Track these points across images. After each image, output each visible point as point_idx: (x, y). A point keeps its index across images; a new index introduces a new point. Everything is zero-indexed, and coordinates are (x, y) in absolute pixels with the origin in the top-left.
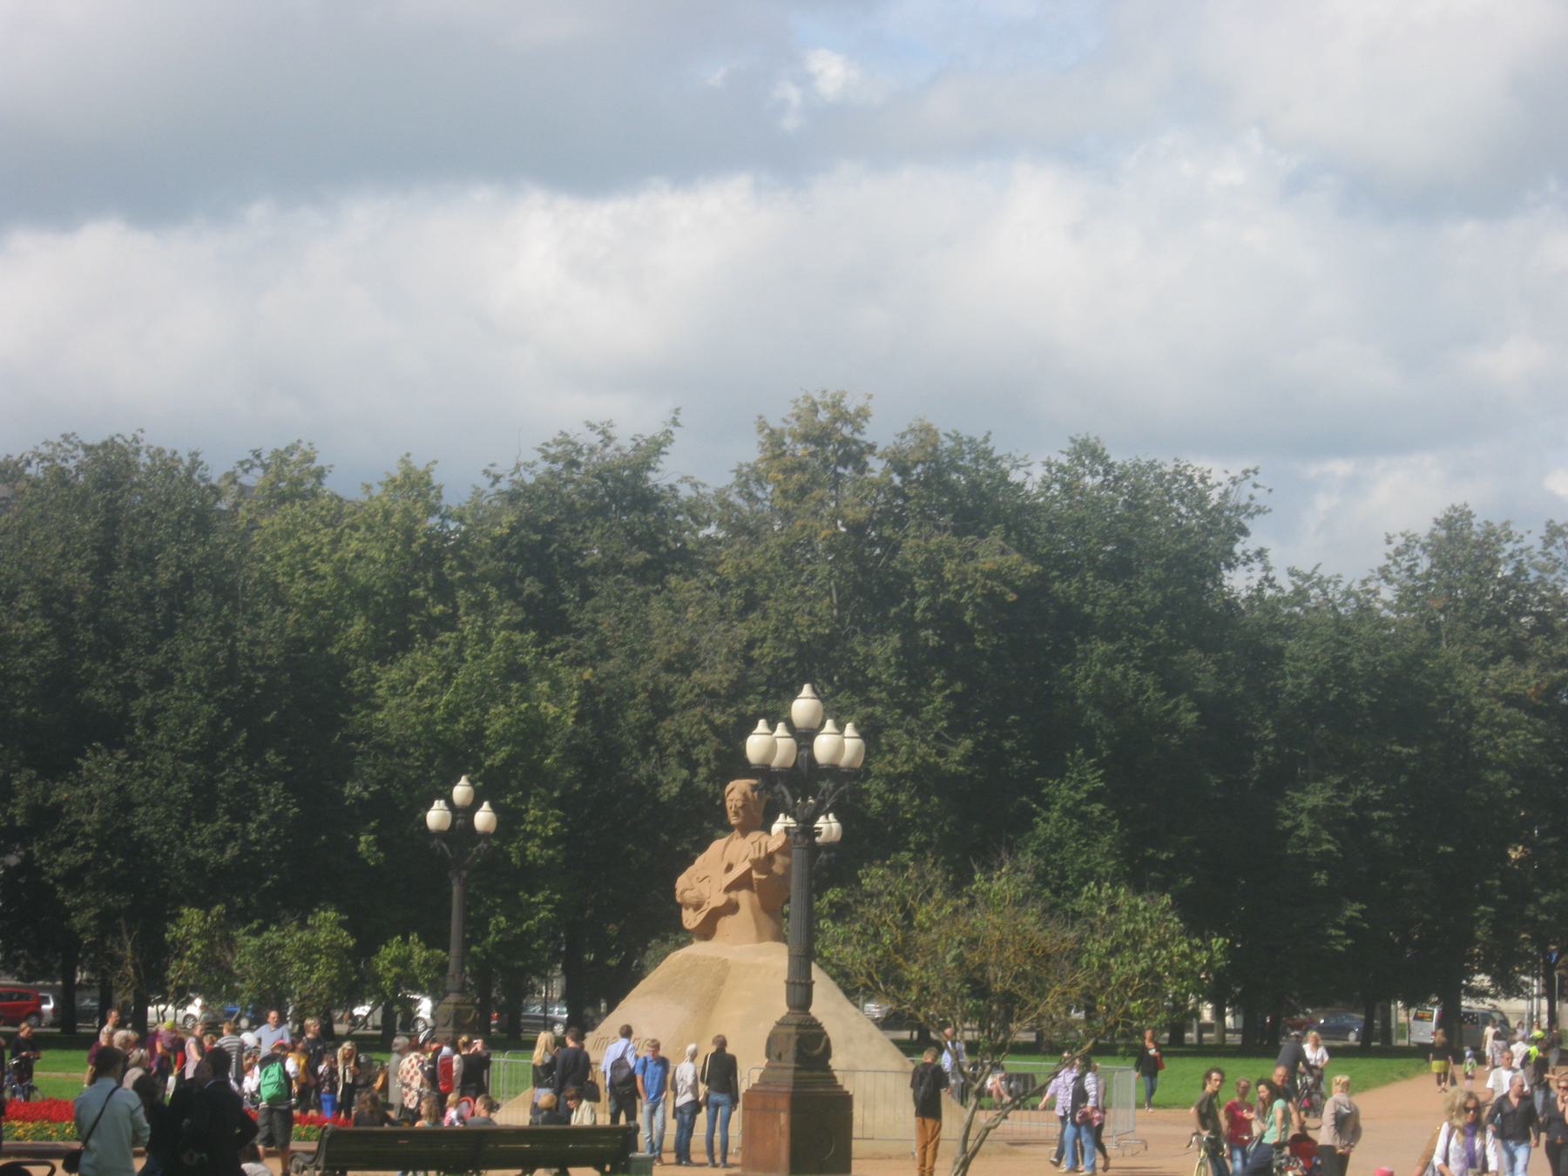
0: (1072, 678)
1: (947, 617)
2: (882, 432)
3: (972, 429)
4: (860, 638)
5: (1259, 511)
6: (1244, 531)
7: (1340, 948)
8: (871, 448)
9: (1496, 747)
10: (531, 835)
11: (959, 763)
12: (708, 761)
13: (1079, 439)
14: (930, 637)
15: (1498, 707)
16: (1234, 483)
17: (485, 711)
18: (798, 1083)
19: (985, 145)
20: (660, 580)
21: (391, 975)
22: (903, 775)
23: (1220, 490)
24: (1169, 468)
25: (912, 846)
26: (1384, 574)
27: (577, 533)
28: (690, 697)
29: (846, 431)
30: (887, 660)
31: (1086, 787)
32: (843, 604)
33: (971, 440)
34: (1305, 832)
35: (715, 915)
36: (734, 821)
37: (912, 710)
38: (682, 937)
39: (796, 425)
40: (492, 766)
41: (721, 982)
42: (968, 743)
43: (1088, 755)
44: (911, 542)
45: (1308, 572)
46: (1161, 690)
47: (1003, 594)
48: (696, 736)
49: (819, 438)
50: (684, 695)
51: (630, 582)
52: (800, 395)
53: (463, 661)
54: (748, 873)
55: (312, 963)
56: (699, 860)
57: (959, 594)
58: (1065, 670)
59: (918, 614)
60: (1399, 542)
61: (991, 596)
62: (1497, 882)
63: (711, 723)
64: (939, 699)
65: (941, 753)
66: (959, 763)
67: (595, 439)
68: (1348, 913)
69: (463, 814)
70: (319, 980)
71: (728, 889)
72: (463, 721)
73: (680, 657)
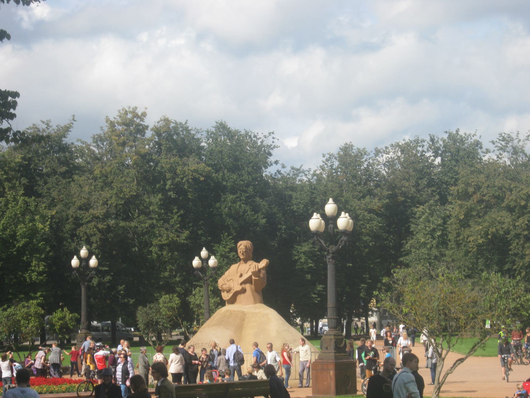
0: (220, 208)
1: (178, 188)
2: (152, 121)
3: (181, 120)
4: (146, 196)
5: (274, 147)
6: (270, 154)
7: (316, 302)
8: (147, 127)
9: (366, 227)
10: (33, 271)
11: (184, 240)
12: (97, 242)
13: (219, 122)
14: (172, 194)
15: (366, 213)
16: (265, 137)
17: (16, 227)
18: (336, 358)
19: (95, 31)
20: (70, 177)
21: (59, 324)
22: (164, 245)
23: (261, 140)
24: (243, 132)
25: (168, 270)
26: (322, 168)
27: (40, 161)
28: (89, 219)
29: (138, 121)
30: (157, 203)
31: (228, 247)
32: (138, 184)
33: (181, 123)
34: (303, 260)
35: (237, 294)
36: (242, 257)
37: (166, 221)
38: (222, 303)
39: (119, 120)
40: (19, 246)
41: (243, 320)
42: (188, 232)
43: (228, 236)
44: (163, 160)
45: (298, 167)
46: (252, 211)
47: (199, 178)
48: (92, 233)
49: (127, 124)
50: (86, 218)
51: (60, 178)
52: (121, 108)
53: (8, 208)
54: (250, 277)
55: (29, 320)
56: (227, 273)
57: (182, 179)
58: (218, 205)
59: (167, 187)
60: (327, 156)
61: (195, 179)
62: (368, 276)
63: (98, 228)
64: (176, 217)
65: (178, 236)
66: (184, 240)
67: (44, 126)
68: (319, 289)
69: (84, 261)
70: (32, 326)
71: (241, 284)
72: (8, 230)
73: (84, 205)
